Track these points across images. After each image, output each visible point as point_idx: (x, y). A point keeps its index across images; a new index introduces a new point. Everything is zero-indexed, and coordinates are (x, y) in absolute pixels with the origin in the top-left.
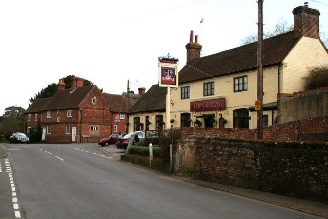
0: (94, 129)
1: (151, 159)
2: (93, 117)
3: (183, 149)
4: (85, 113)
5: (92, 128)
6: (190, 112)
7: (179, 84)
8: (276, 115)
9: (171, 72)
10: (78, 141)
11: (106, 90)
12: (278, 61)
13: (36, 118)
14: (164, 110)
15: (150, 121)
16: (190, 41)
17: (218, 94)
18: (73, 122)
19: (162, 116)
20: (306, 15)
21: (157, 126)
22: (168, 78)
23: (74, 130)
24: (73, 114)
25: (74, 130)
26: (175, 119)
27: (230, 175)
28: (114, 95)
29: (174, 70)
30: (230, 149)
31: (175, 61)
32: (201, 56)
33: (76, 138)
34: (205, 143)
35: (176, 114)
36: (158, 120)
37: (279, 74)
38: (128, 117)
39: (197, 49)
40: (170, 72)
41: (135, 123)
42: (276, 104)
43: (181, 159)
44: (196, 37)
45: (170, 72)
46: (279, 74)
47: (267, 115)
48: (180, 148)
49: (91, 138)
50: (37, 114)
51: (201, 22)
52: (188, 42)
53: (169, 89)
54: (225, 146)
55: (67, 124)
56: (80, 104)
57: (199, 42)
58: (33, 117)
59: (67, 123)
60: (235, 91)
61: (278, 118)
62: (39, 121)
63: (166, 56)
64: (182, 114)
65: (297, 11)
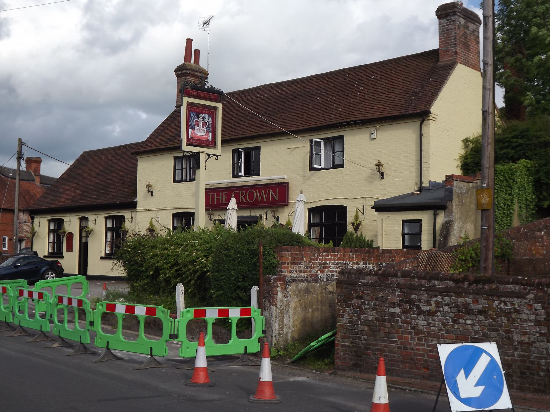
3: (286, 296)
7: (224, 142)
8: (441, 219)
9: (206, 120)
11: (143, 138)
12: (422, 108)
14: (132, 206)
16: (185, 60)
19: (124, 217)
20: (463, 21)
30: (460, 300)
34: (372, 285)
35: (160, 213)
36: (52, 227)
37: (421, 135)
38: (33, 218)
40: (204, 118)
42: (441, 193)
43: (282, 321)
44: (197, 52)
45: (204, 118)
47: (420, 221)
48: (280, 295)
51: (206, 23)
52: (181, 62)
53: (203, 157)
54: (446, 292)
57: (203, 64)
60: (175, 182)
61: (447, 227)
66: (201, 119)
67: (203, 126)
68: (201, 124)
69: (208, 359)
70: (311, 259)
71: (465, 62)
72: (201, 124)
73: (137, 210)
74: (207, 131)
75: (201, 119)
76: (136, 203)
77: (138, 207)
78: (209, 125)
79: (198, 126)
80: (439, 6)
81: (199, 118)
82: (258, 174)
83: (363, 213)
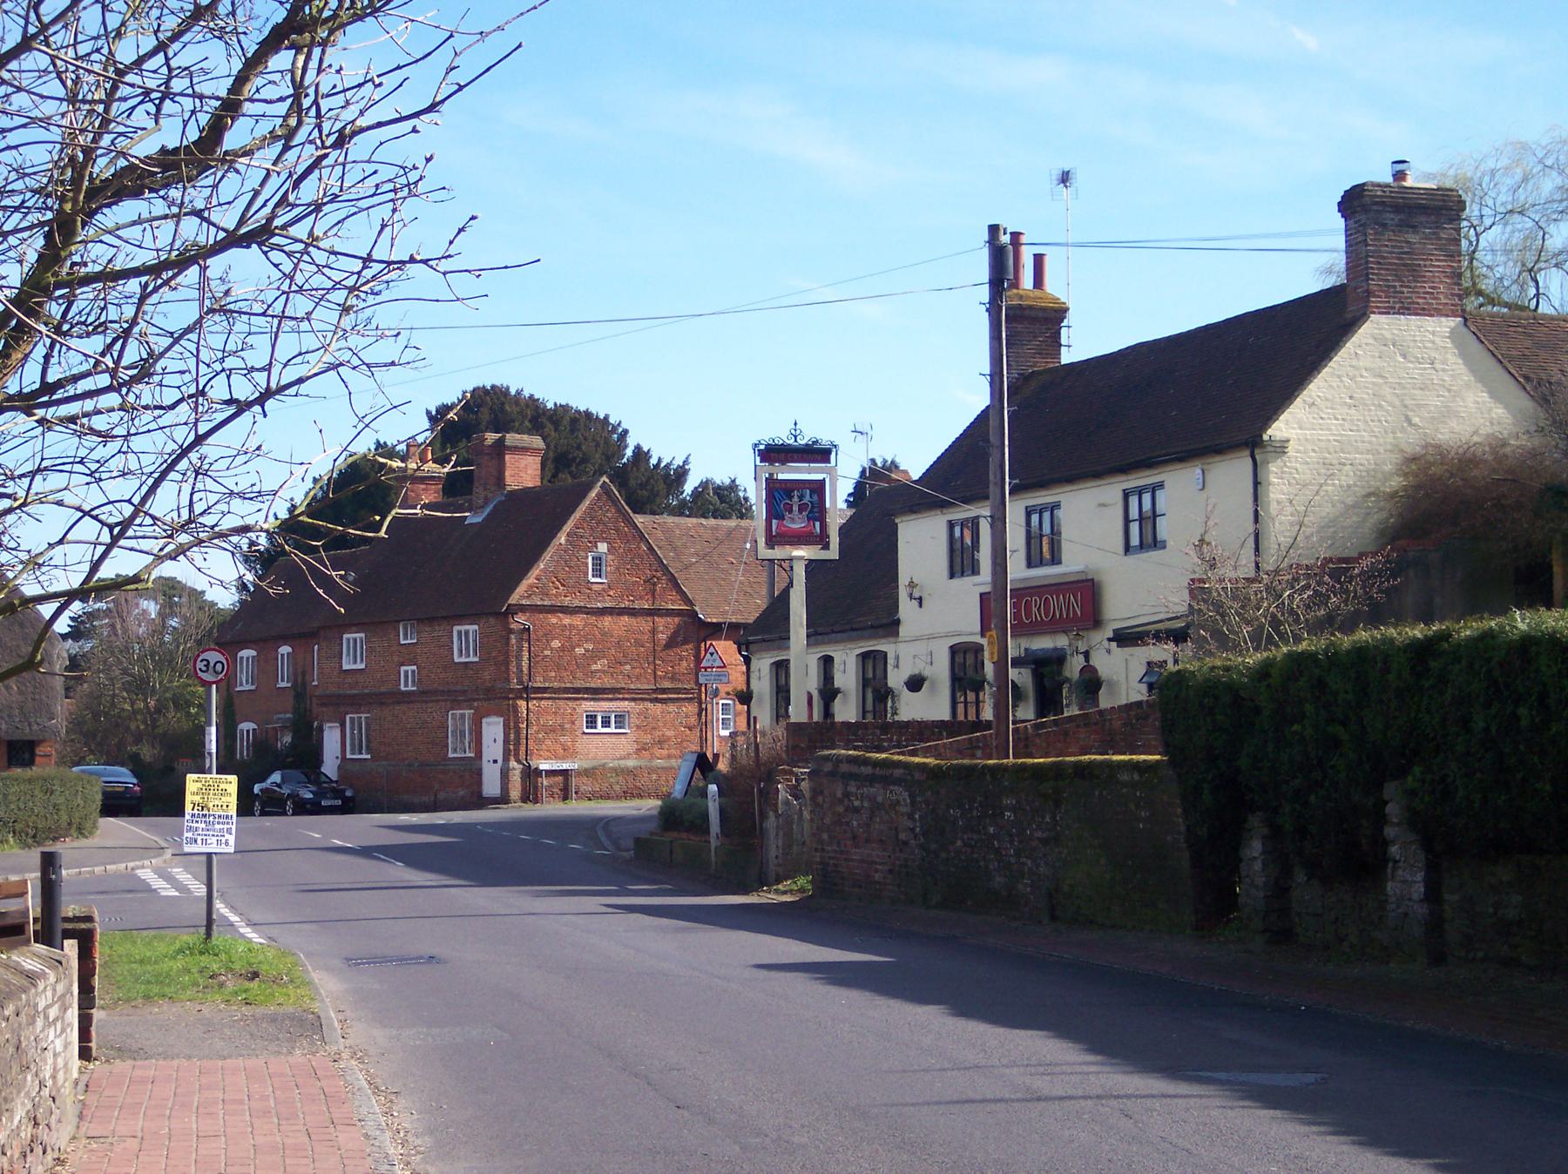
0: (606, 723)
1: (714, 843)
2: (592, 656)
4: (549, 636)
5: (591, 721)
6: (978, 639)
9: (807, 499)
10: (515, 793)
13: (284, 669)
14: (891, 627)
15: (839, 681)
17: (1074, 561)
18: (488, 690)
21: (869, 706)
22: (797, 523)
23: (493, 729)
24: (484, 647)
25: (493, 729)
26: (926, 673)
27: (876, 871)
28: (1096, 357)
29: (818, 488)
31: (819, 453)
32: (1067, 357)
33: (505, 774)
37: (1256, 484)
39: (1047, 320)
40: (801, 497)
41: (865, 683)
45: (801, 497)
46: (1256, 484)
49: (586, 773)
50: (285, 650)
55: (456, 704)
56: (522, 588)
57: (1054, 286)
58: (266, 664)
59: (455, 698)
60: (1127, 549)
62: (300, 690)
63: (782, 435)
64: (954, 650)
65: (1354, 203)
66: (796, 499)
67: (800, 511)
68: (795, 508)
69: (257, 813)
70: (849, 740)
71: (1400, 308)
72: (795, 508)
73: (900, 639)
74: (809, 519)
75: (796, 499)
76: (897, 622)
77: (902, 630)
78: (813, 507)
79: (791, 511)
80: (1345, 192)
81: (791, 498)
82: (1059, 562)
83: (897, 666)
